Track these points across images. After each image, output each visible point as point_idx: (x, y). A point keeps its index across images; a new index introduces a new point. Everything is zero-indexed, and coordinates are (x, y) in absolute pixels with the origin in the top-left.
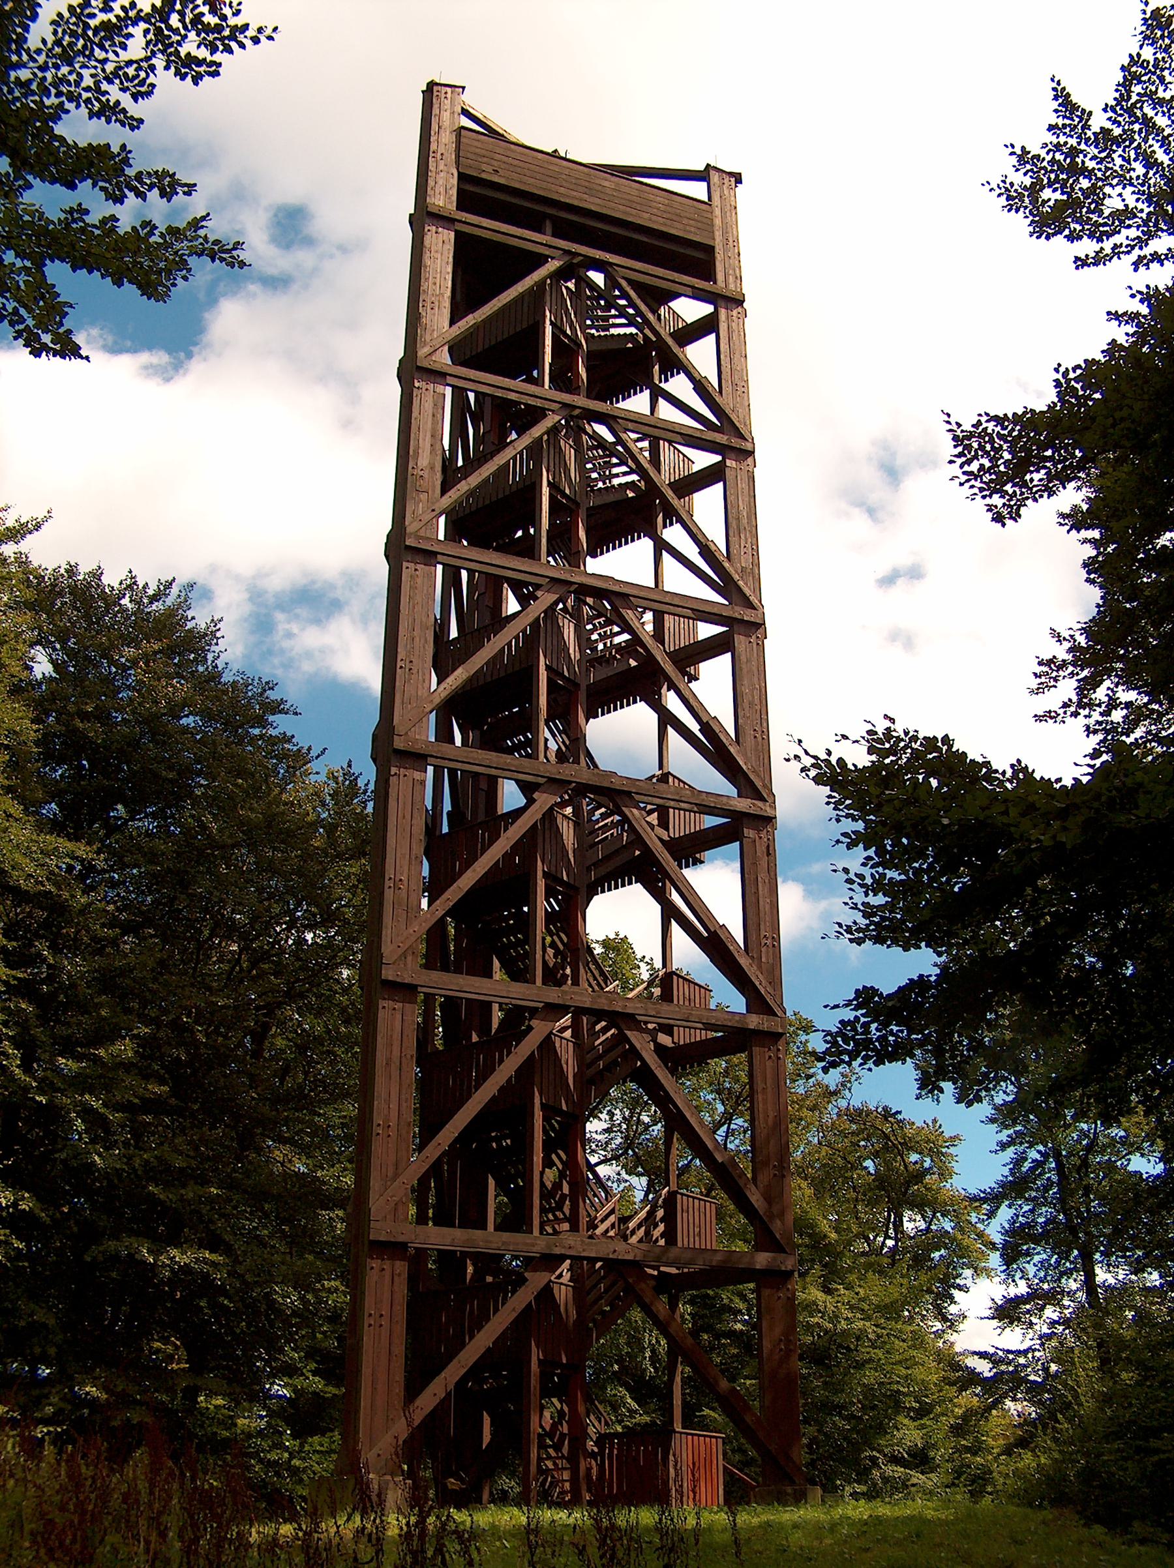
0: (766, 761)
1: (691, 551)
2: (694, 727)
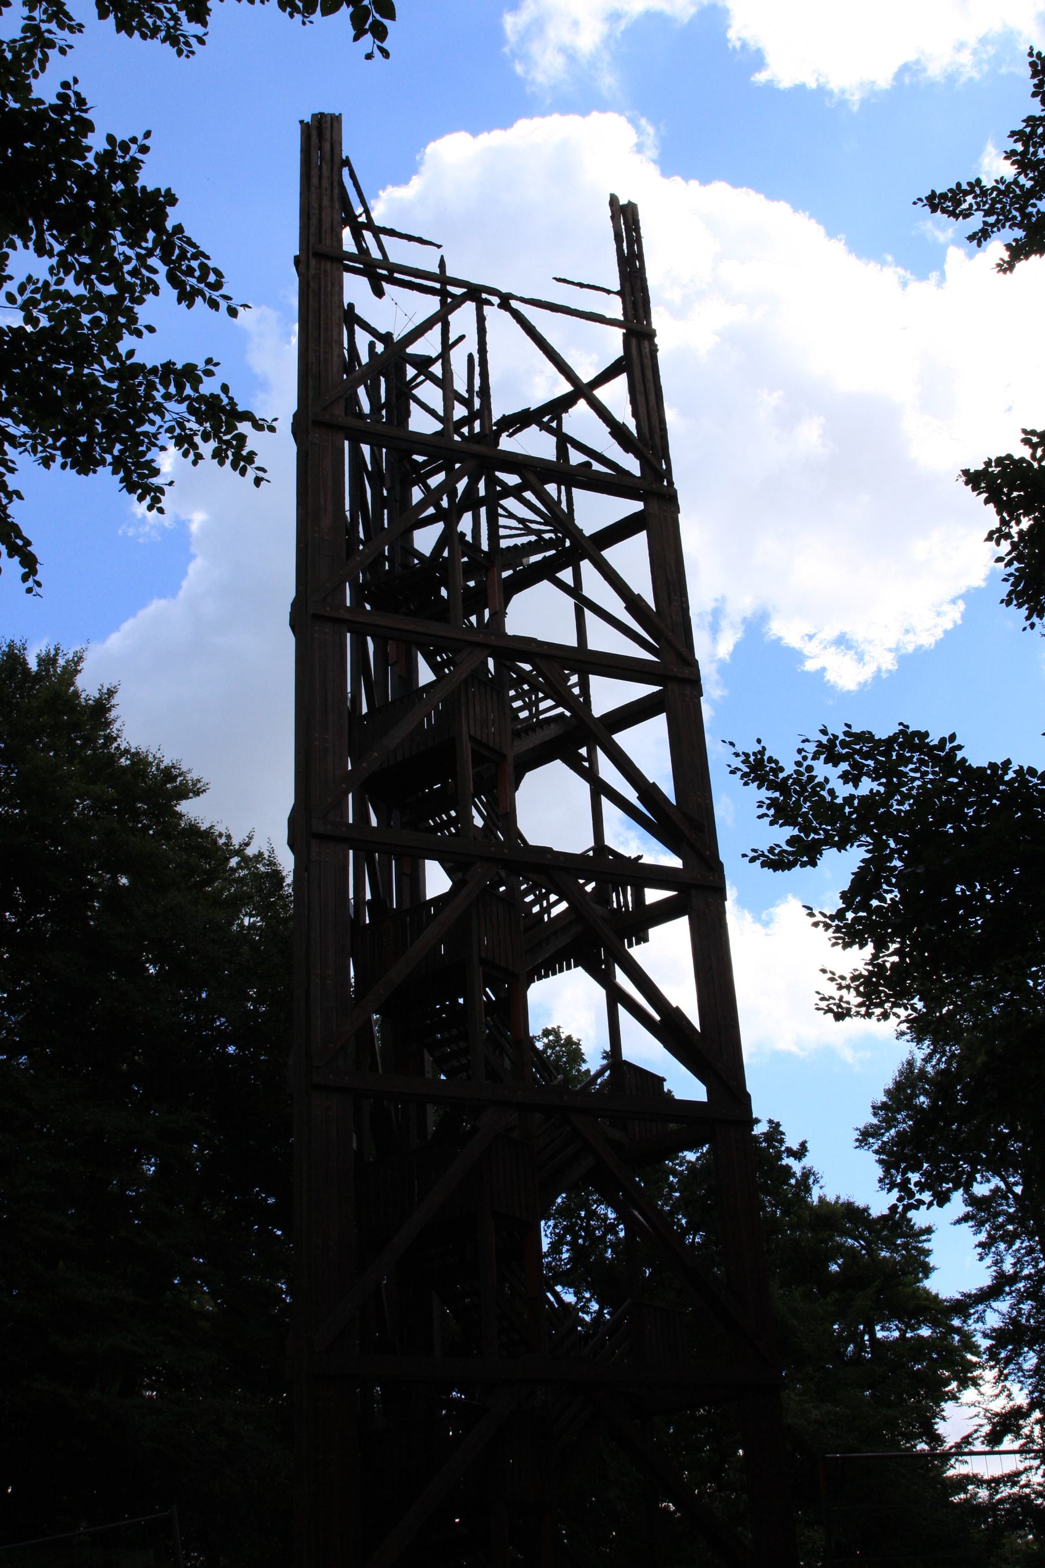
0: (651, 386)
1: (616, 606)
2: (631, 795)
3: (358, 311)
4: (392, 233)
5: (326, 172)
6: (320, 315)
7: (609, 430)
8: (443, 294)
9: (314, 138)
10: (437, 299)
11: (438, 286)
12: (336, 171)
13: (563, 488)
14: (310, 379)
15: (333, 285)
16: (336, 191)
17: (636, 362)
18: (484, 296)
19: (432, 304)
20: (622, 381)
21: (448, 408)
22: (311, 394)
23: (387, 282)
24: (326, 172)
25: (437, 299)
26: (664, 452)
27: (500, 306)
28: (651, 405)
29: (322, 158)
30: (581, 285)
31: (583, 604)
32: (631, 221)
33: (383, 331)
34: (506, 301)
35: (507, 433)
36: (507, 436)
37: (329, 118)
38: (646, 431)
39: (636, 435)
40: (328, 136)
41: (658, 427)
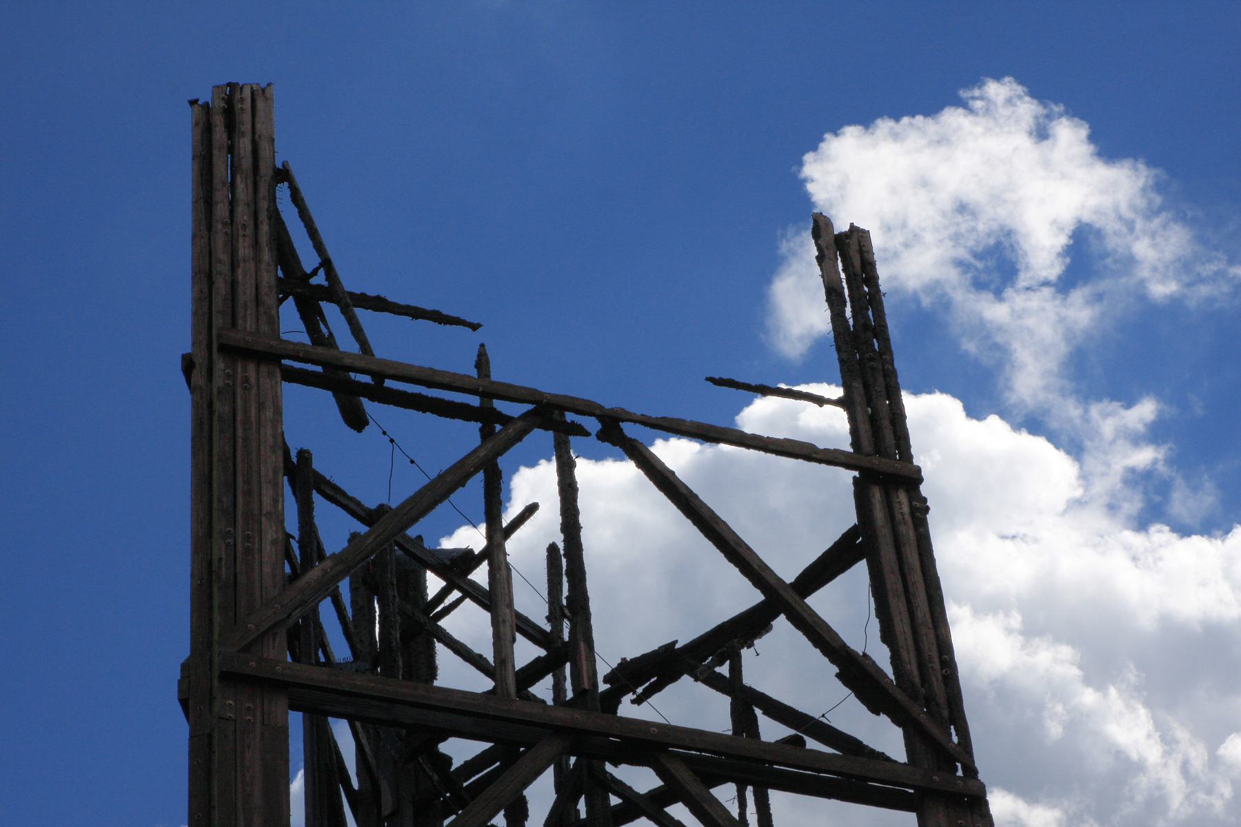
0: (917, 577)
3: (318, 465)
4: (379, 304)
5: (243, 190)
6: (235, 465)
7: (836, 670)
8: (486, 417)
9: (220, 133)
10: (475, 426)
11: (474, 401)
12: (263, 190)
13: (749, 792)
14: (215, 589)
15: (261, 406)
16: (265, 228)
17: (884, 533)
18: (570, 417)
19: (466, 436)
20: (859, 573)
21: (502, 644)
22: (217, 619)
23: (372, 399)
24: (243, 190)
25: (475, 426)
28: (919, 614)
29: (235, 169)
32: (857, 262)
33: (371, 503)
35: (631, 696)
36: (633, 702)
37: (247, 93)
38: (913, 667)
39: (892, 677)
40: (247, 127)
41: (937, 660)
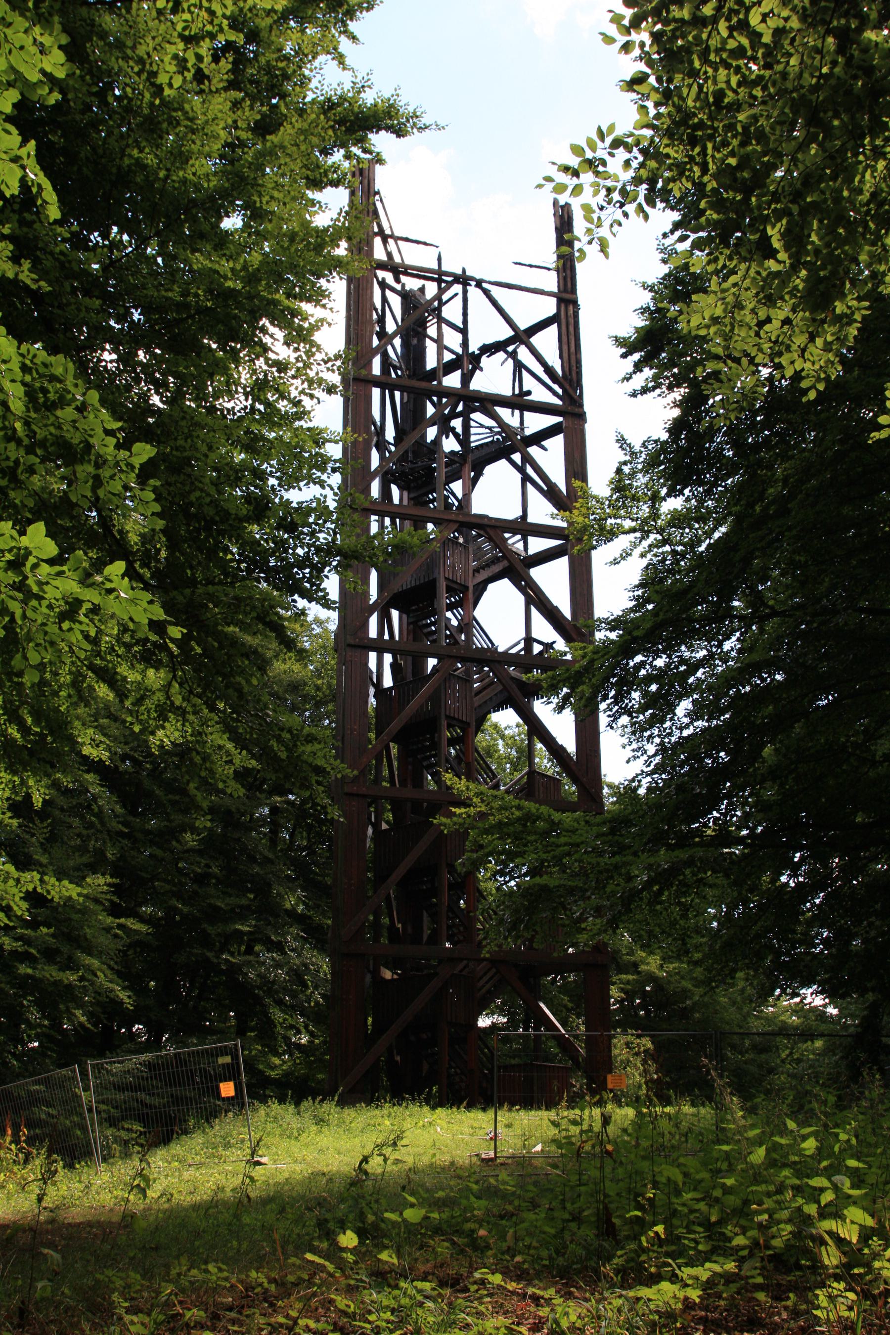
0: (571, 329)
1: (539, 370)
4: (407, 240)
8: (439, 281)
26: (579, 384)
27: (477, 286)
30: (531, 266)
31: (519, 367)
34: (479, 284)
38: (567, 369)
